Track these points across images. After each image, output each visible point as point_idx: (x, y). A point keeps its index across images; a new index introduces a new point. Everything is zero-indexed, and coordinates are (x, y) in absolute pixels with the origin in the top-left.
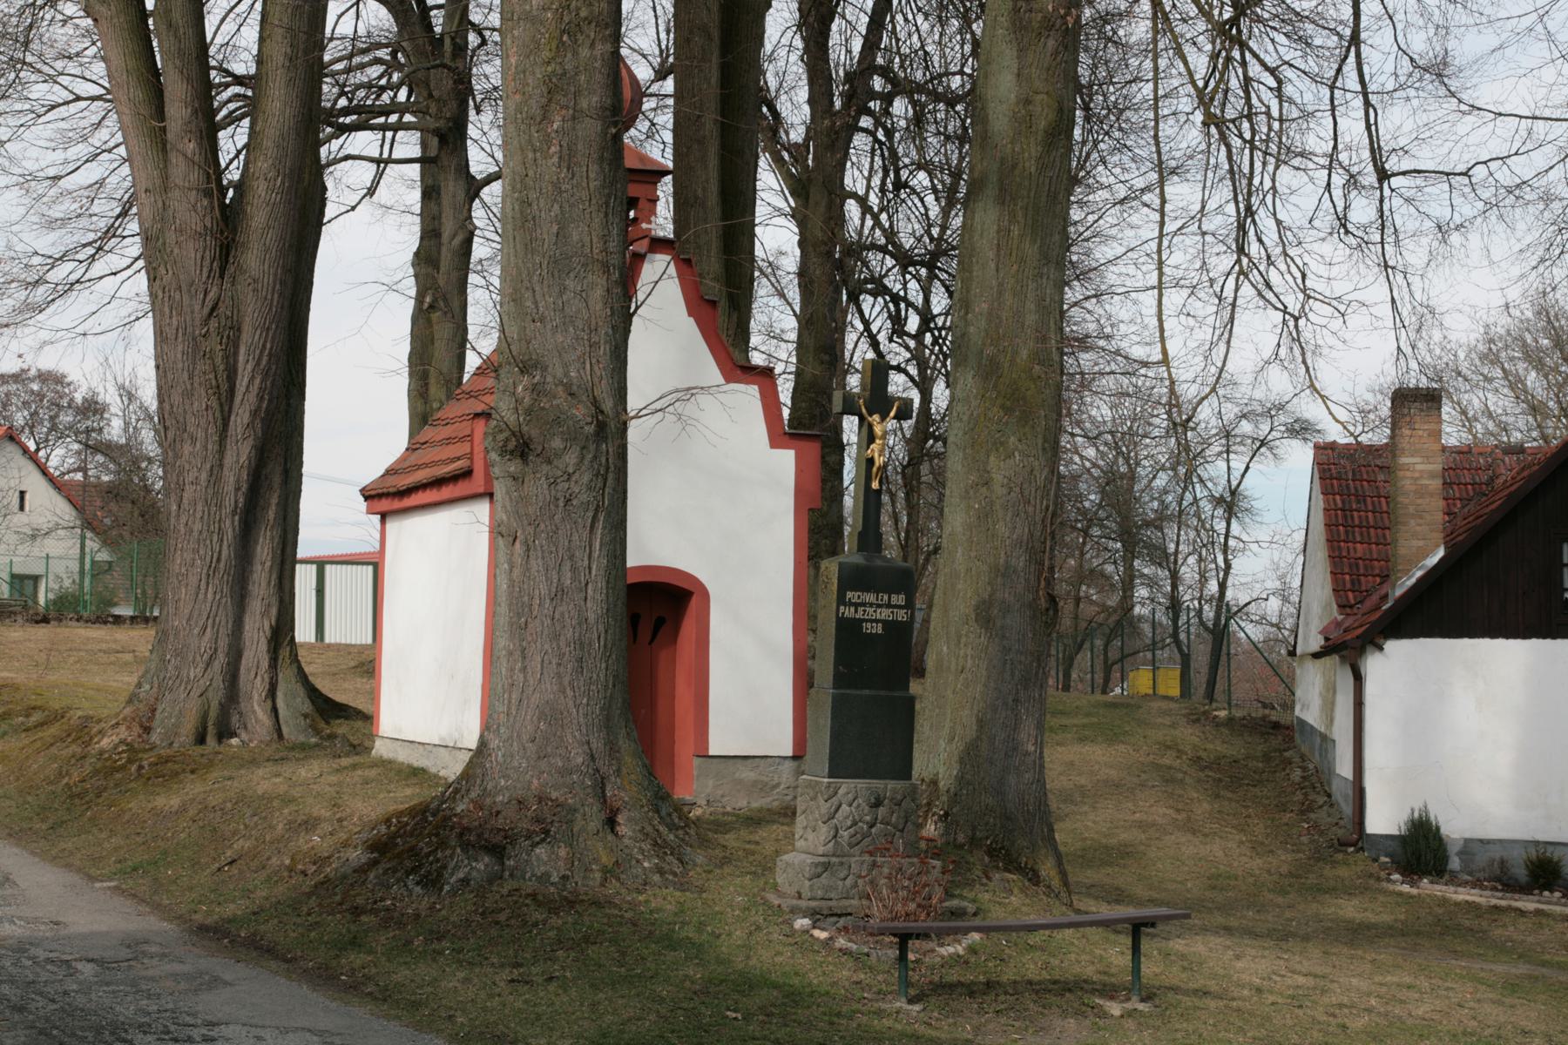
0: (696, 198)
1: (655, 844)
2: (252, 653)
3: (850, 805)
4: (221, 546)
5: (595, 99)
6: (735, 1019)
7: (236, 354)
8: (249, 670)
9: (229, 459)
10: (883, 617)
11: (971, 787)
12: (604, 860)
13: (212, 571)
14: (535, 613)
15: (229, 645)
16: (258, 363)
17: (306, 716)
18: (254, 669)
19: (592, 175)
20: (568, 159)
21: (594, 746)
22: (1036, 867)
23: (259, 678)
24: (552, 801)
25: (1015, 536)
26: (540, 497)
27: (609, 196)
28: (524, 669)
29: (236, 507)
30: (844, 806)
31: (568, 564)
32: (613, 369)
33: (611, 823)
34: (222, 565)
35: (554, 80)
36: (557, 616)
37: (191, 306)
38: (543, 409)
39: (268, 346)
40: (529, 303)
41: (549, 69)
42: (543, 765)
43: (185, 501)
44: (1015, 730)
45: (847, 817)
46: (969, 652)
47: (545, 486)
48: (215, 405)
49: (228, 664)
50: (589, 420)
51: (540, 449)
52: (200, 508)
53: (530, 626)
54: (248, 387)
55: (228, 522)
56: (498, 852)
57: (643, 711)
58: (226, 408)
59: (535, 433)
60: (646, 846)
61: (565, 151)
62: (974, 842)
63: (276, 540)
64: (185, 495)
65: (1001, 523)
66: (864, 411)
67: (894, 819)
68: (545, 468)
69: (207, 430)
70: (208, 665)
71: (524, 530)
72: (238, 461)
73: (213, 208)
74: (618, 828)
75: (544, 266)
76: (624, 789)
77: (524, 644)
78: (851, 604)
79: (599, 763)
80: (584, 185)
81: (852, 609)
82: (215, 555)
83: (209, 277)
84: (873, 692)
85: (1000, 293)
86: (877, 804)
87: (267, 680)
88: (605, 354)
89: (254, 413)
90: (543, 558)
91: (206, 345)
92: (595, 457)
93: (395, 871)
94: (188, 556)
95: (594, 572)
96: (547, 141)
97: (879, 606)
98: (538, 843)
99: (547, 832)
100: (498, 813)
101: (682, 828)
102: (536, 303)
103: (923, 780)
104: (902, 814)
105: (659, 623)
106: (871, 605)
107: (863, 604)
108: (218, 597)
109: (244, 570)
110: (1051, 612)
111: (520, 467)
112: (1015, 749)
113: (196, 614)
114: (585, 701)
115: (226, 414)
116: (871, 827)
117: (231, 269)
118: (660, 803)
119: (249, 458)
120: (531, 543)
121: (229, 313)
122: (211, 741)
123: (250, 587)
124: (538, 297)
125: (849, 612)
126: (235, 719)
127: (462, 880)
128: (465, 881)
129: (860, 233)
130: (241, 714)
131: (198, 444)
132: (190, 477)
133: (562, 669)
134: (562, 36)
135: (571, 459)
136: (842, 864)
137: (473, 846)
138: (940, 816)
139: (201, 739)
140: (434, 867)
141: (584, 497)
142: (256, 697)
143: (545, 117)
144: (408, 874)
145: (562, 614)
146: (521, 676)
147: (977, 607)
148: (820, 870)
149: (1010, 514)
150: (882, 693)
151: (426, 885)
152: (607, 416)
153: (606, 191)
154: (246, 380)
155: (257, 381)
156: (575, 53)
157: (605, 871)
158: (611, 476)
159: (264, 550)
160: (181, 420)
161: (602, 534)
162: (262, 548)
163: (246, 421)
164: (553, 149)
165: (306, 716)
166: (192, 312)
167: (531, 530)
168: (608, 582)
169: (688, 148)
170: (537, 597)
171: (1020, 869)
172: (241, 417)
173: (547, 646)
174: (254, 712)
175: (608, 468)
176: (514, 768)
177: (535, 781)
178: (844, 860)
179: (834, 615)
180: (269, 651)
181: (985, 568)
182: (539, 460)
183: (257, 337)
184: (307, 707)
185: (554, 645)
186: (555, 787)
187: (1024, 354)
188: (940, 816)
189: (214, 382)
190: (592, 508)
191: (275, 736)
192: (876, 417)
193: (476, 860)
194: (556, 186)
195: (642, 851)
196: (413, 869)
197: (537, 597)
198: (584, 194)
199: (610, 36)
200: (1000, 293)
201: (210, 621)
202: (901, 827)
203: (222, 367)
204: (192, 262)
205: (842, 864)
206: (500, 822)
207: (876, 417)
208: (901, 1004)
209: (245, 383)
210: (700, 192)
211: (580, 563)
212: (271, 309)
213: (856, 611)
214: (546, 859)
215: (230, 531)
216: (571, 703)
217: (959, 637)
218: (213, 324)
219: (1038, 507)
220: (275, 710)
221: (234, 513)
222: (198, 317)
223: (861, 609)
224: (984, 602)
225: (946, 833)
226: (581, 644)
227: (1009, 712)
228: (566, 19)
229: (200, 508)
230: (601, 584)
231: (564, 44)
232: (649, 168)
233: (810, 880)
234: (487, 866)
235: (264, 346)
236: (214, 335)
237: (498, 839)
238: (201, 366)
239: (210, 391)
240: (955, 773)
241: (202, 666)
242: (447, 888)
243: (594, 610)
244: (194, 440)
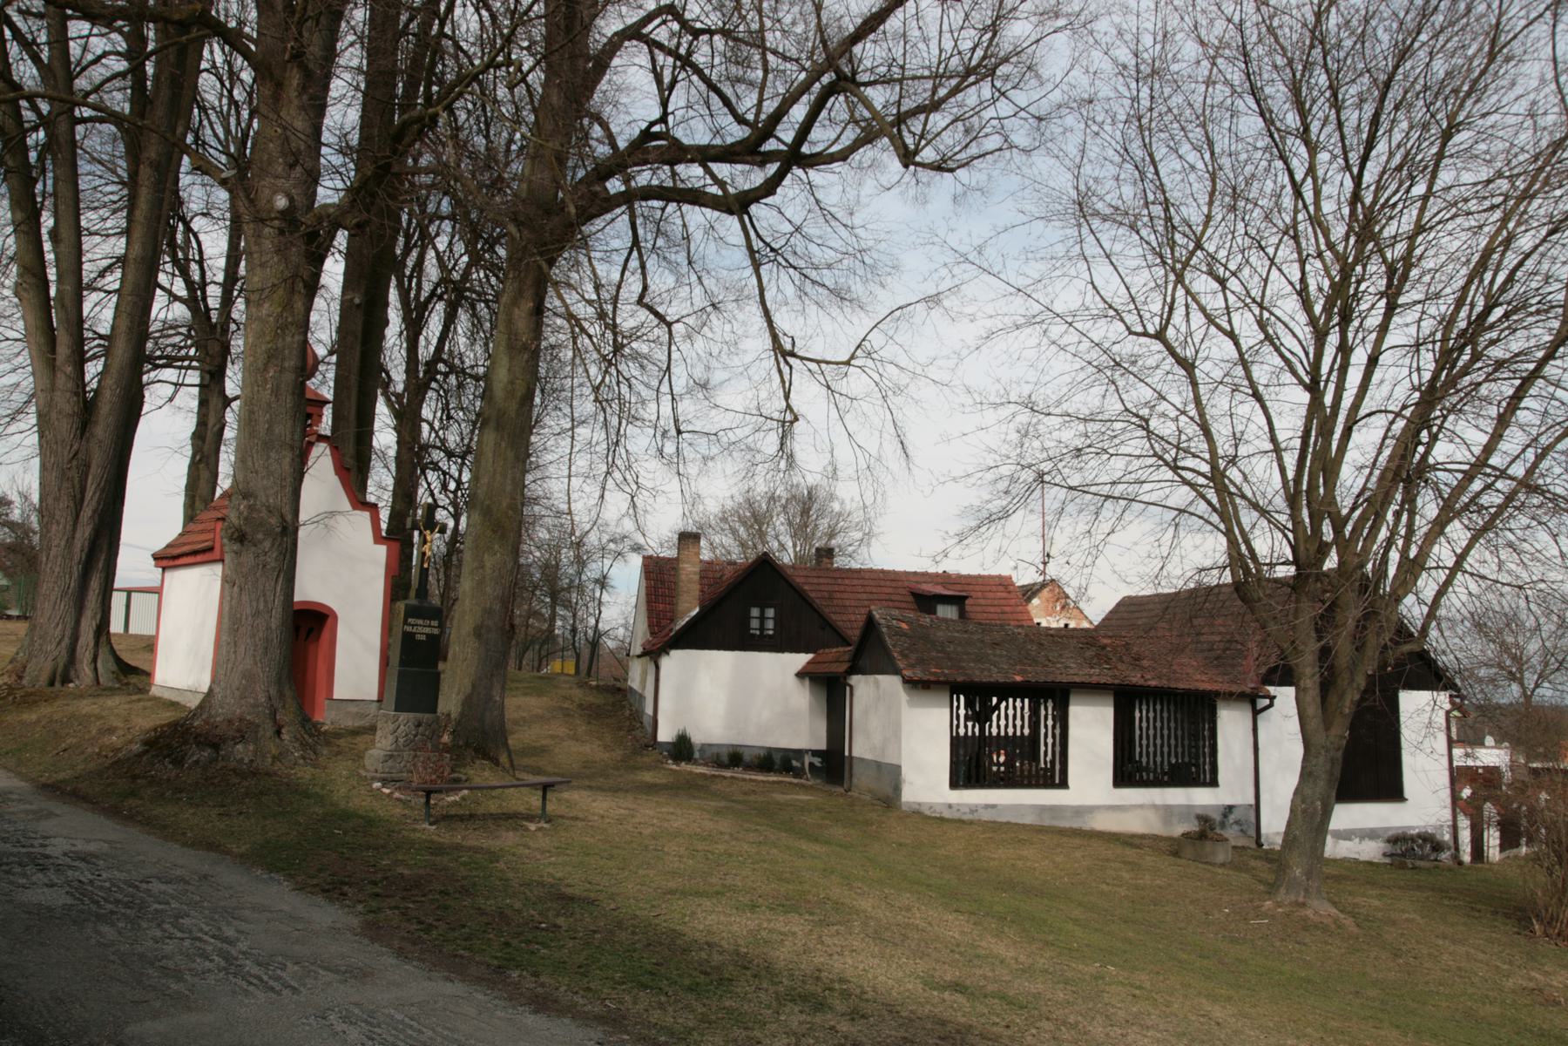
9: (78, 535)
13: (64, 593)
20: (276, 392)
28: (235, 652)
33: (278, 733)
42: (243, 702)
56: (216, 747)
60: (297, 745)
62: (467, 745)
68: (253, 549)
86: (419, 725)
89: (94, 512)
96: (266, 383)
99: (243, 737)
105: (310, 631)
122: (57, 685)
125: (409, 629)
126: (72, 673)
139: (52, 683)
141: (273, 564)
143: (266, 369)
157: (274, 757)
159: (95, 584)
172: (87, 513)
187: (504, 505)
194: (269, 404)
220: (96, 669)
225: (453, 740)
226: (267, 640)
230: (280, 610)
243: (275, 623)
244: (58, 523)
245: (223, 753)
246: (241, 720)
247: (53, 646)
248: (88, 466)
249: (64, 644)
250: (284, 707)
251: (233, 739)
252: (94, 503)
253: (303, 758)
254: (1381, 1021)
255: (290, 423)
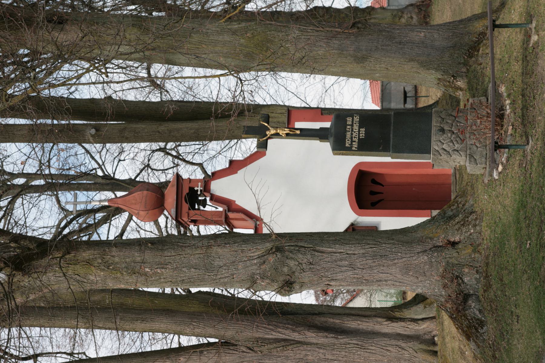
0: (195, 133)
1: (463, 225)
2: (398, 329)
3: (443, 144)
4: (351, 344)
5: (136, 254)
6: (530, 244)
7: (269, 339)
8: (405, 331)
9: (314, 341)
10: (357, 128)
11: (440, 65)
12: (470, 251)
13: (362, 347)
14: (361, 276)
15: (395, 339)
16: (272, 330)
17: (425, 307)
18: (405, 328)
19: (169, 254)
20: (163, 265)
21: (420, 250)
22: (478, 33)
23: (409, 326)
24: (444, 273)
25: (324, 46)
26: (309, 276)
27: (178, 246)
28: (386, 281)
29: (334, 337)
30: (444, 147)
31: (338, 262)
32: (253, 243)
33: (454, 244)
34: (360, 343)
35: (129, 272)
36: (362, 267)
37: (249, 357)
38: (271, 275)
39: (265, 326)
40: (226, 280)
41: (125, 273)
42: (428, 274)
43: (333, 358)
44: (414, 43)
45: (449, 145)
46: (378, 66)
47: (305, 274)
48: (290, 347)
49: (403, 340)
50: (275, 255)
51: (288, 277)
52: (335, 352)
53: (366, 278)
54: (282, 334)
55: (341, 341)
56: (467, 297)
57: (414, 189)
58: (292, 342)
59: (282, 278)
60: (464, 229)
61: (160, 266)
62: (465, 64)
63: (349, 319)
64: (330, 358)
65: (319, 52)
66: (265, 138)
67: (450, 122)
68: (296, 274)
69: (302, 350)
70: (403, 349)
71: (324, 281)
72: (315, 337)
73: (208, 350)
74: (456, 241)
75: (209, 274)
76: (439, 236)
77: (375, 280)
78: (351, 144)
79: (428, 248)
80: (173, 257)
81: (354, 143)
82: (356, 346)
83: (237, 351)
84: (392, 132)
85: (216, 53)
86: (442, 130)
87: (409, 323)
88: (246, 247)
89: (294, 331)
90: (336, 273)
91: (266, 352)
92: (291, 252)
93: (477, 336)
94: (356, 357)
95: (342, 251)
96: (156, 273)
97: (352, 130)
98: (462, 281)
99: (457, 277)
100: (449, 296)
101: (458, 205)
102: (225, 277)
103: (438, 83)
104: (448, 117)
105: (374, 182)
106: (352, 134)
107: (352, 138)
108: (374, 345)
109: (362, 333)
110: (360, 25)
111: (296, 284)
112: (423, 42)
113: (382, 354)
114: (400, 254)
115: (294, 342)
116: (453, 133)
117: (233, 341)
118: (447, 215)
119: (313, 332)
120: (330, 279)
121: (251, 343)
122: (436, 349)
123: (369, 330)
124: (223, 276)
125: (355, 145)
126: (427, 337)
127: (480, 312)
128: (480, 311)
129: (167, 232)
130: (425, 334)
131: (308, 353)
132: (322, 356)
133: (386, 265)
134: (111, 269)
135: (292, 263)
136: (470, 149)
137: (464, 307)
138: (454, 79)
139: (435, 353)
140: (475, 321)
141: (309, 257)
142: (417, 328)
143: (146, 274)
144: (478, 332)
145: (361, 265)
146: (389, 282)
147: (357, 63)
148: (472, 160)
149: (315, 48)
150: (392, 128)
151: (482, 325)
152: (273, 246)
153: (176, 247)
154: (280, 335)
155: (280, 330)
156: (117, 263)
157: (474, 251)
158: (300, 244)
159: (352, 324)
160: (298, 360)
161: (326, 247)
162: (352, 325)
163: (297, 334)
164: (159, 271)
165: (425, 307)
166: (252, 357)
167: (324, 279)
168: (347, 244)
169: (173, 137)
170: (353, 276)
171: (479, 42)
172: (295, 336)
173: (375, 271)
174: (424, 328)
175: (297, 246)
176: (430, 286)
177: (435, 278)
178: (468, 148)
179: (357, 152)
180: (397, 322)
181: (339, 59)
182: (293, 277)
183: (261, 331)
184: (421, 306)
185: (375, 268)
186: (438, 270)
187: (242, 41)
188: (454, 79)
189: (281, 348)
190: (313, 253)
191: (434, 320)
192: (268, 133)
193: (471, 306)
194: (175, 269)
195: (466, 232)
196: (476, 329)
197: (353, 276)
198: (178, 257)
199: (109, 249)
200: (216, 53)
201: (384, 348)
202: (454, 118)
203: (275, 345)
204: (231, 357)
205: (470, 149)
206: (454, 296)
207: (268, 133)
208: (528, 148)
209: (281, 335)
210: (192, 131)
211: (338, 257)
212: (249, 325)
213: (355, 142)
214: (469, 278)
215: (345, 340)
216: (400, 261)
217: (371, 70)
218: (255, 349)
219: (311, 34)
220: (423, 319)
221: (337, 338)
222: (254, 354)
223: (354, 139)
224: (355, 60)
225: (462, 77)
226: (374, 257)
227: (406, 47)
228: (103, 267)
229: (335, 352)
230: (347, 247)
231: (113, 268)
232: (176, 183)
233: (477, 164)
234: (473, 302)
235: (265, 328)
236: (261, 349)
237: (461, 298)
238: (274, 353)
239: (285, 349)
240: (433, 72)
241: (403, 351)
242: (483, 319)
243: (359, 250)
244: (306, 355)
245: (472, 292)
246: (443, 277)
247: (406, 352)
248: (257, 340)
249: (403, 345)
250: (431, 239)
251: (459, 285)
252: (287, 332)
253: (475, 226)
254: (472, 90)
255: (188, 251)
